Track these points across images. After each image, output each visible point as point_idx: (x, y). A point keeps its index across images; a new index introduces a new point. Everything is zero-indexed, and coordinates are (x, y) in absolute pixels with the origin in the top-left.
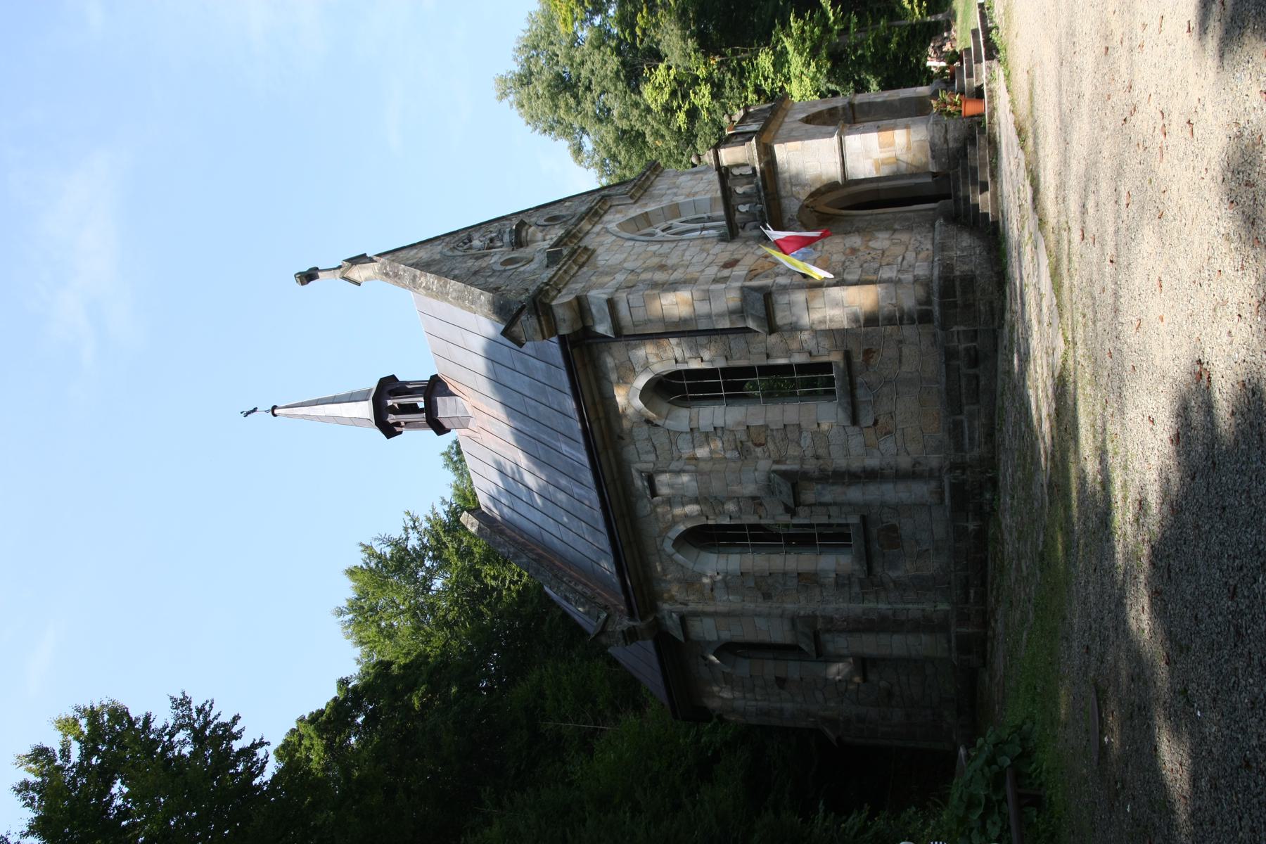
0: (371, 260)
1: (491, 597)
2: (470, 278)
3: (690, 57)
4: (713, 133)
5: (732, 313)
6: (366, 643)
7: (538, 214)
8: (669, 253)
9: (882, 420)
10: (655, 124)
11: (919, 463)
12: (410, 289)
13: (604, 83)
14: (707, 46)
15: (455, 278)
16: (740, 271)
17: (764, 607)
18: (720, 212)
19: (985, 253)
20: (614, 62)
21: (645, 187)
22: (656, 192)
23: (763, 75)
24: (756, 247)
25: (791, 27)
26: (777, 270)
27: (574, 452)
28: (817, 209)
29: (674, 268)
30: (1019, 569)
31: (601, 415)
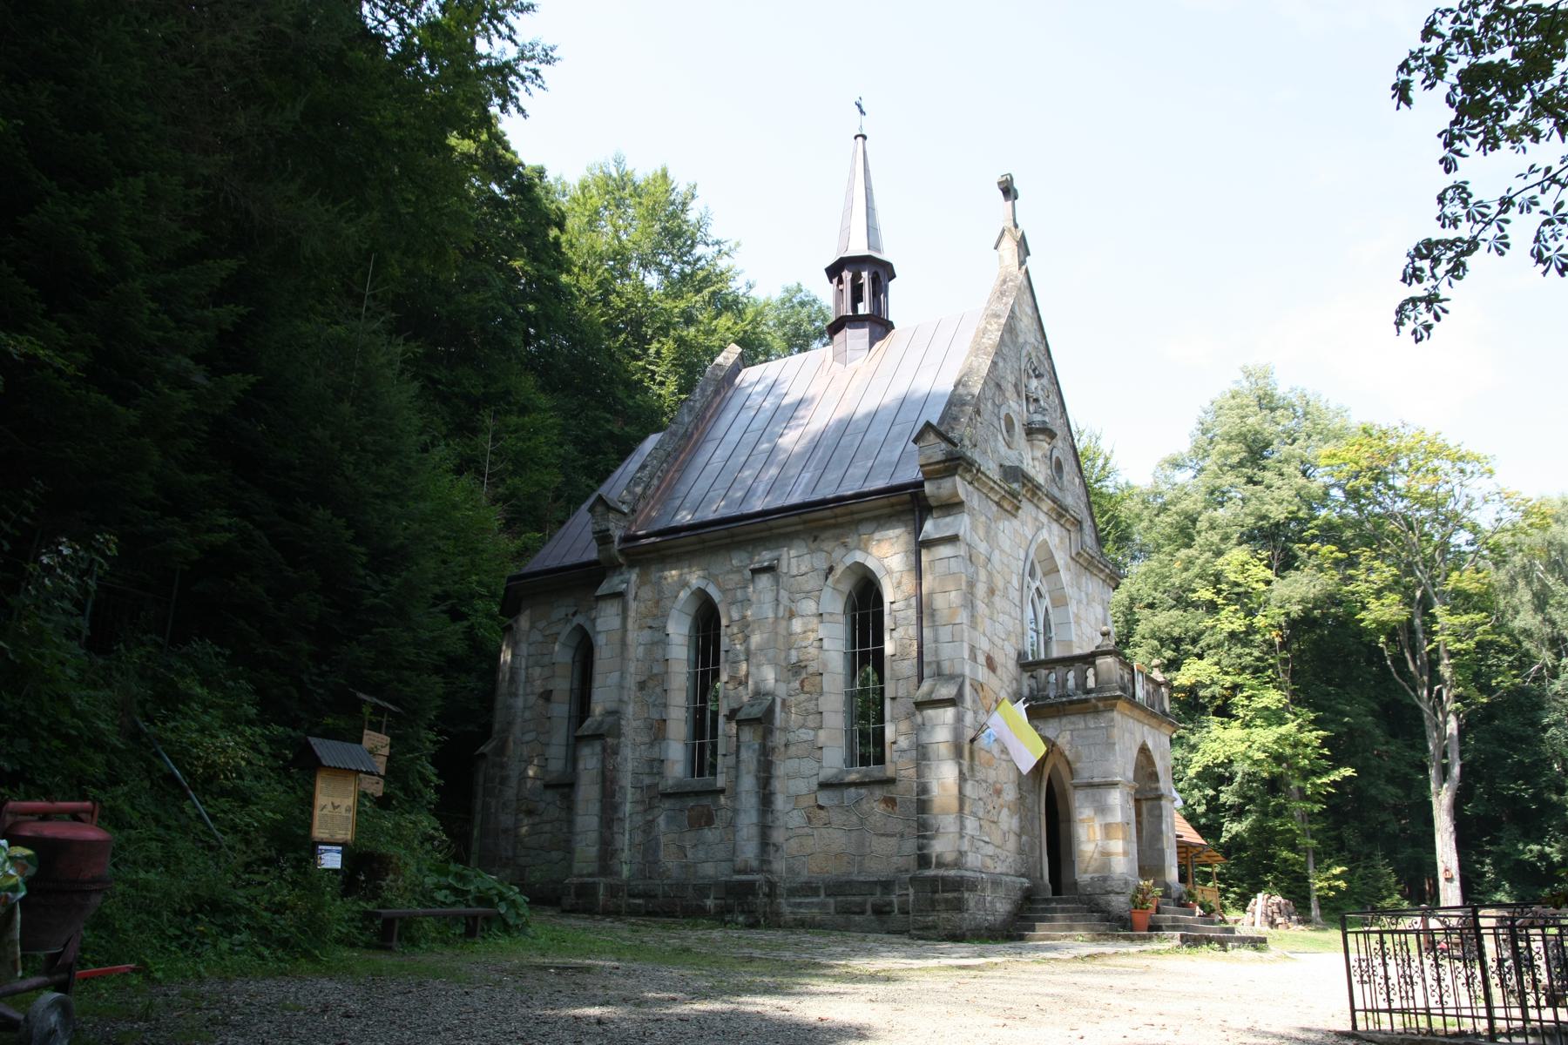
0: (1022, 263)
1: (636, 347)
6: (583, 194)
7: (1067, 448)
8: (1008, 598)
9: (823, 813)
12: (986, 309)
13: (1254, 501)
14: (1298, 626)
15: (994, 363)
16: (982, 673)
17: (631, 682)
18: (1056, 653)
20: (1278, 514)
22: (1084, 580)
23: (1253, 696)
25: (1310, 731)
29: (990, 605)
31: (840, 520)
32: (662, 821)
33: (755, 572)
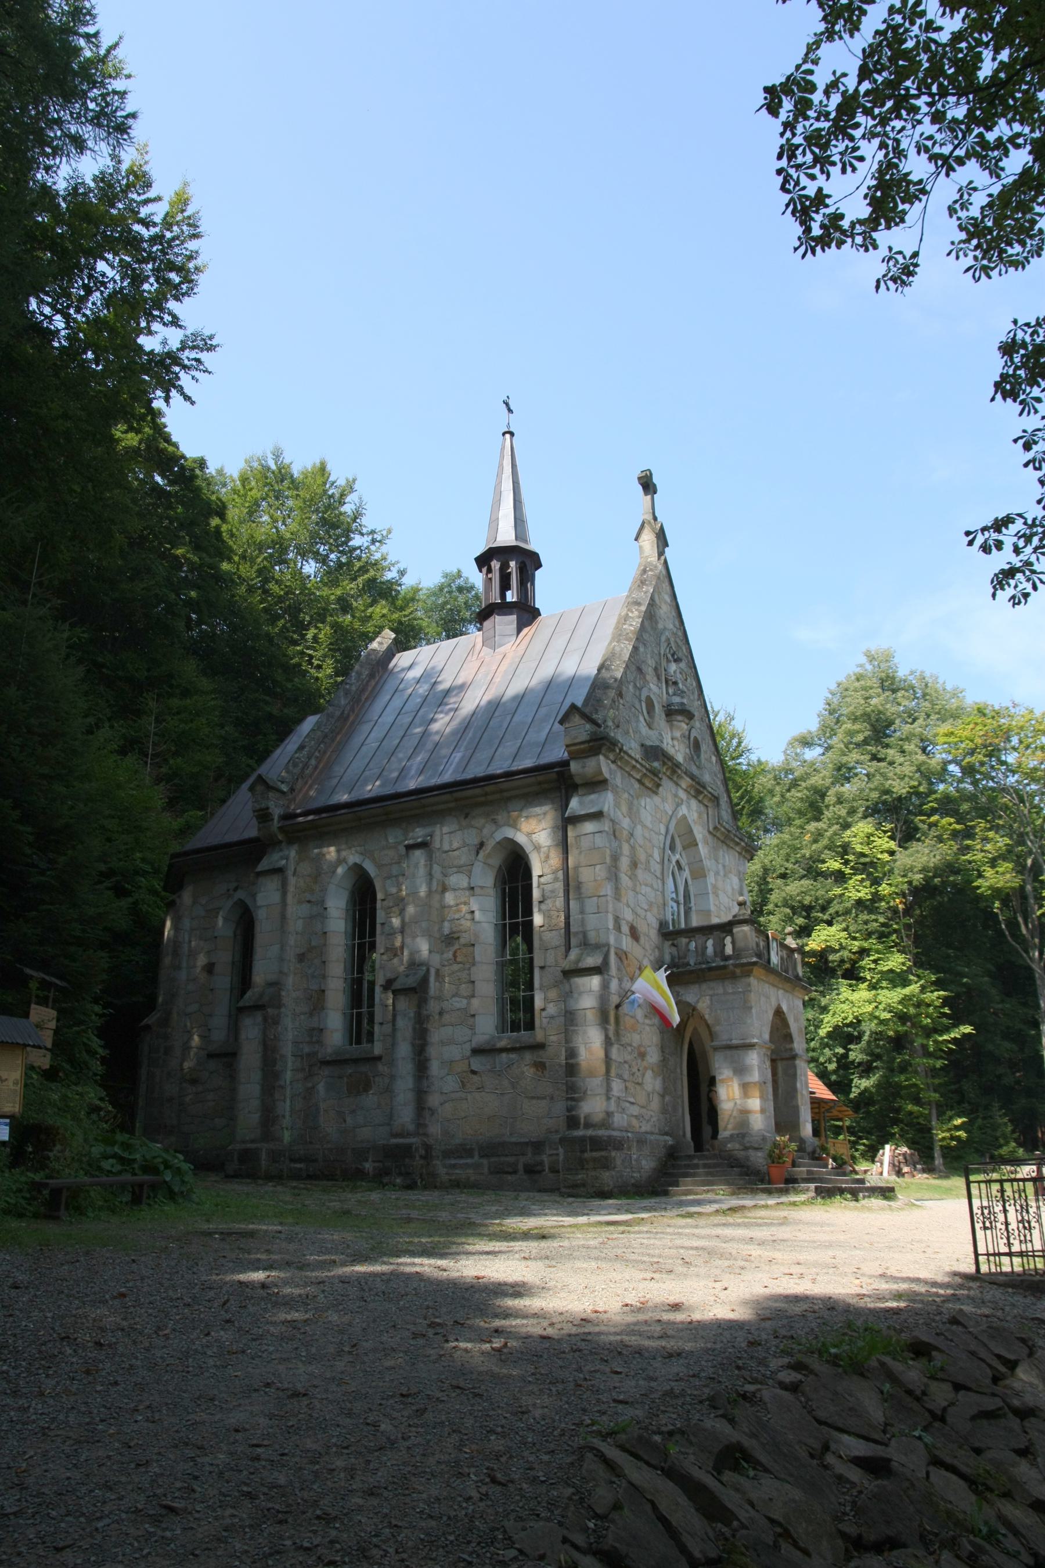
0: (661, 553)
1: (294, 632)
2: (635, 664)
3: (903, 876)
4: (817, 899)
5: (585, 934)
7: (705, 729)
8: (650, 871)
9: (475, 1078)
10: (828, 834)
11: (433, 1114)
12: (627, 597)
15: (635, 649)
16: (626, 943)
18: (695, 922)
19: (633, 1181)
20: (900, 788)
21: (728, 842)
23: (879, 959)
24: (652, 958)
25: (932, 992)
26: (625, 979)
27: (453, 766)
28: (691, 1019)
29: (633, 877)
30: (331, 1201)
31: (490, 798)
32: (321, 1088)
33: (409, 848)
